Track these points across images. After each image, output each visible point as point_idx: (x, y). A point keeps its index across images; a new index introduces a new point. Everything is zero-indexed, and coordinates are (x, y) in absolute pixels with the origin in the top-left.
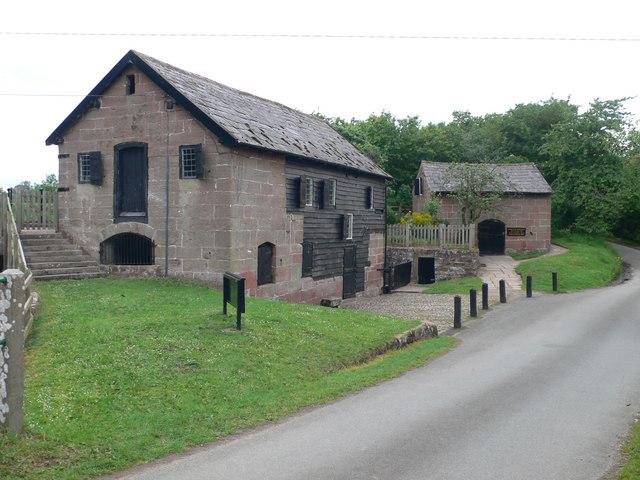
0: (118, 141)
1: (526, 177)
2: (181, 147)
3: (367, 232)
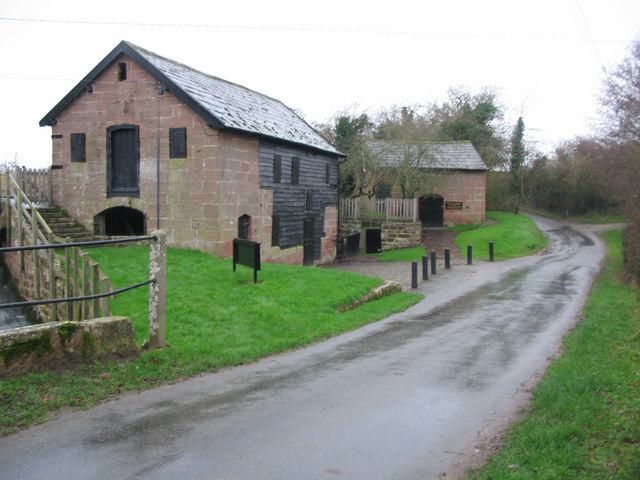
0: (110, 123)
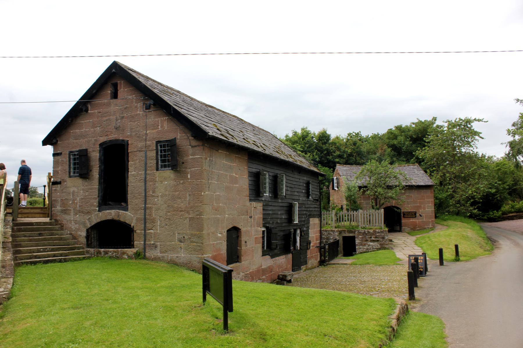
2: (158, 142)
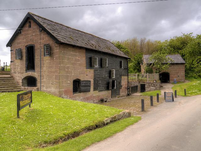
1: (177, 58)
3: (121, 76)
